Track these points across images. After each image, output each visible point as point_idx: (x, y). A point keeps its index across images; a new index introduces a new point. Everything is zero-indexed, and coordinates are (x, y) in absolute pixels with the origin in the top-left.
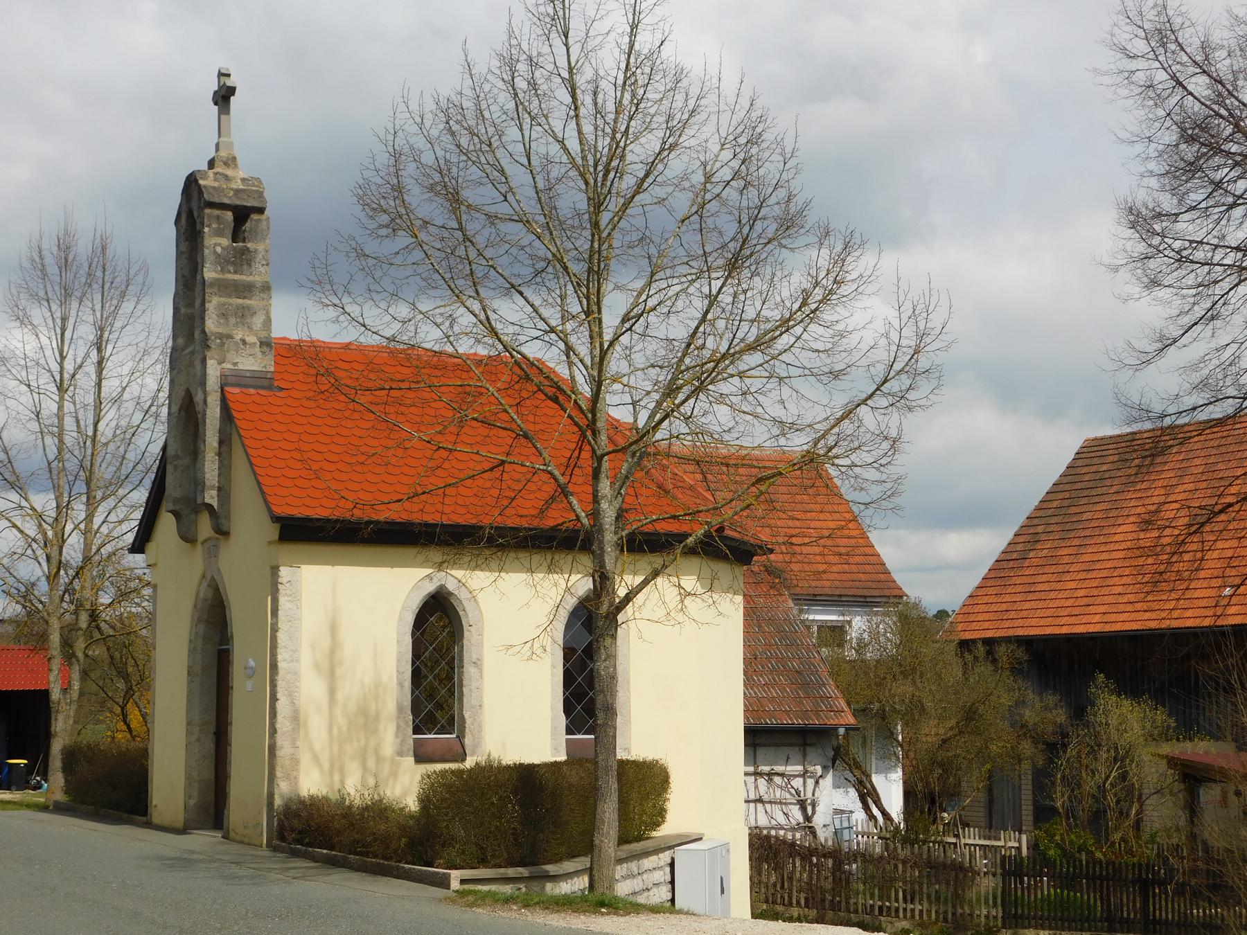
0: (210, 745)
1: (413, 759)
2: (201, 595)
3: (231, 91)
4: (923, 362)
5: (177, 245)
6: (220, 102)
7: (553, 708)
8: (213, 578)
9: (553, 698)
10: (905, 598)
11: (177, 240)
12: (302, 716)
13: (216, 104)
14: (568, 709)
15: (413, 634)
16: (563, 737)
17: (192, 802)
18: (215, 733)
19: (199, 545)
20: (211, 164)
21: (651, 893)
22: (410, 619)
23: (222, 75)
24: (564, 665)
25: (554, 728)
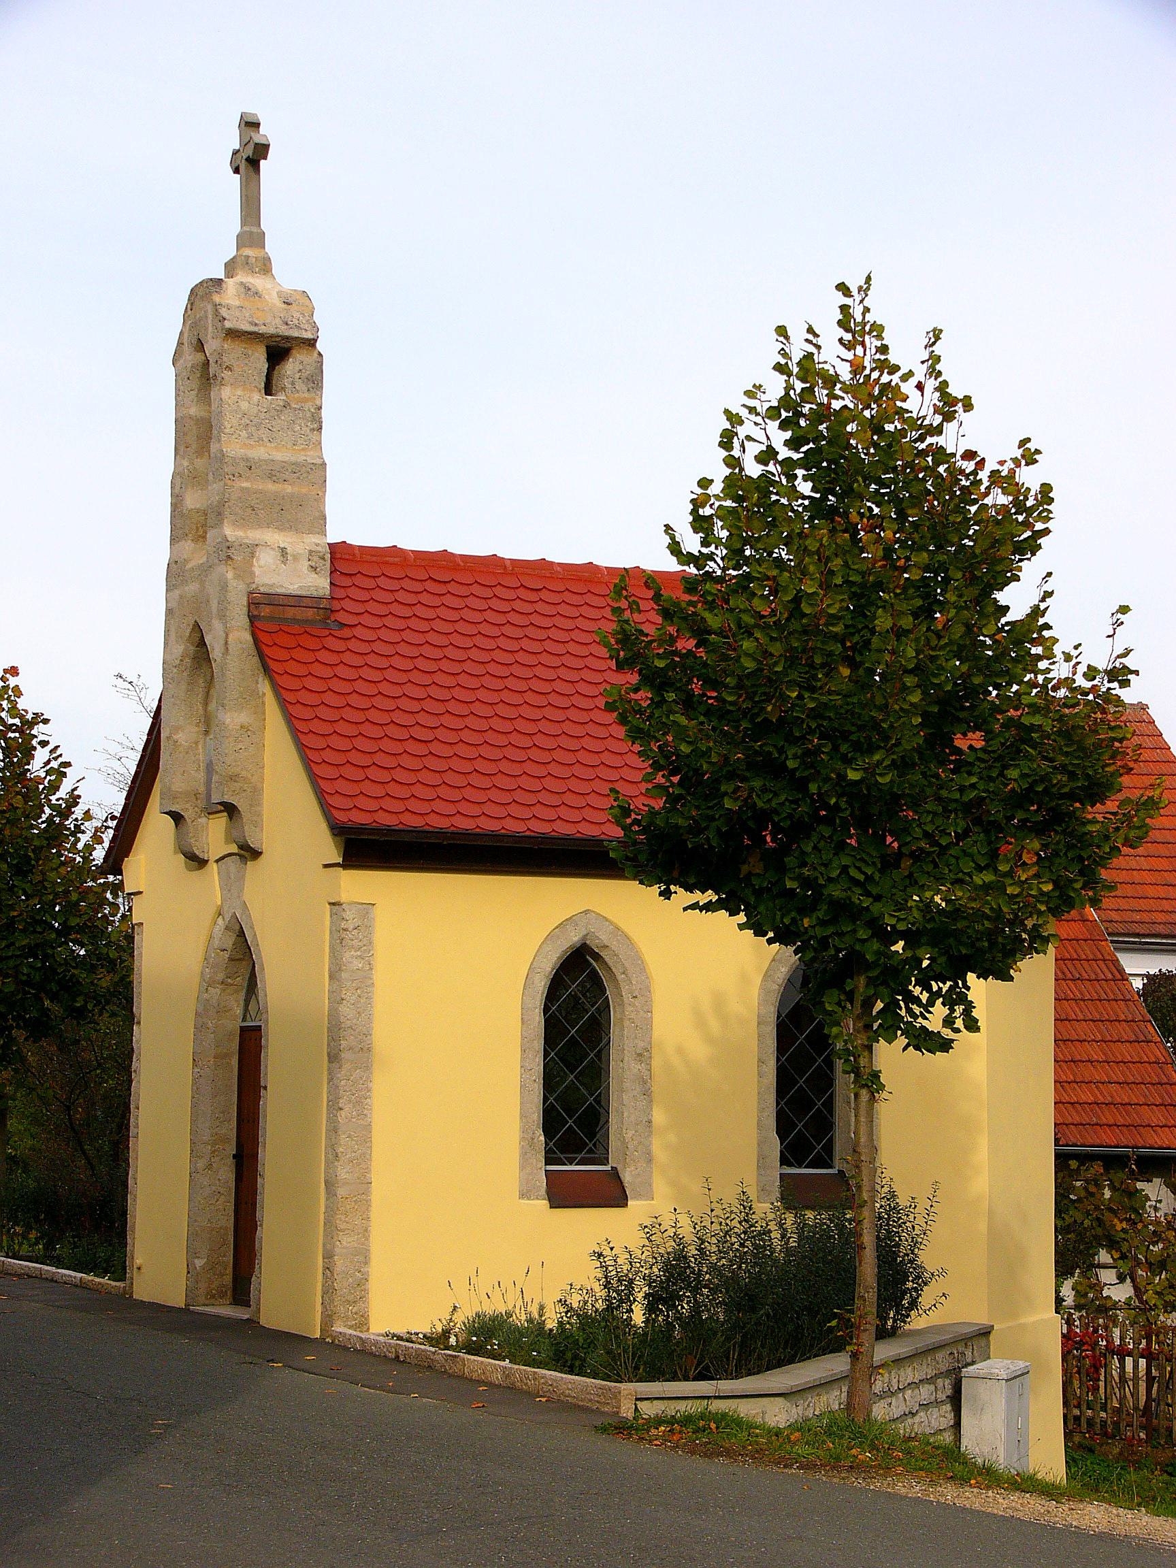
0: (226, 1174)
1: (546, 1202)
2: (216, 943)
3: (262, 150)
4: (234, 848)
5: (177, 395)
6: (242, 169)
7: (760, 1125)
8: (234, 916)
9: (761, 1110)
10: (257, 830)
11: (177, 389)
12: (195, 384)
13: (236, 170)
14: (784, 1126)
15: (546, 1009)
16: (775, 1170)
17: (199, 1263)
18: (234, 1156)
19: (213, 867)
20: (231, 267)
21: (917, 1419)
22: (541, 985)
23: (250, 124)
24: (778, 1060)
25: (762, 1157)
